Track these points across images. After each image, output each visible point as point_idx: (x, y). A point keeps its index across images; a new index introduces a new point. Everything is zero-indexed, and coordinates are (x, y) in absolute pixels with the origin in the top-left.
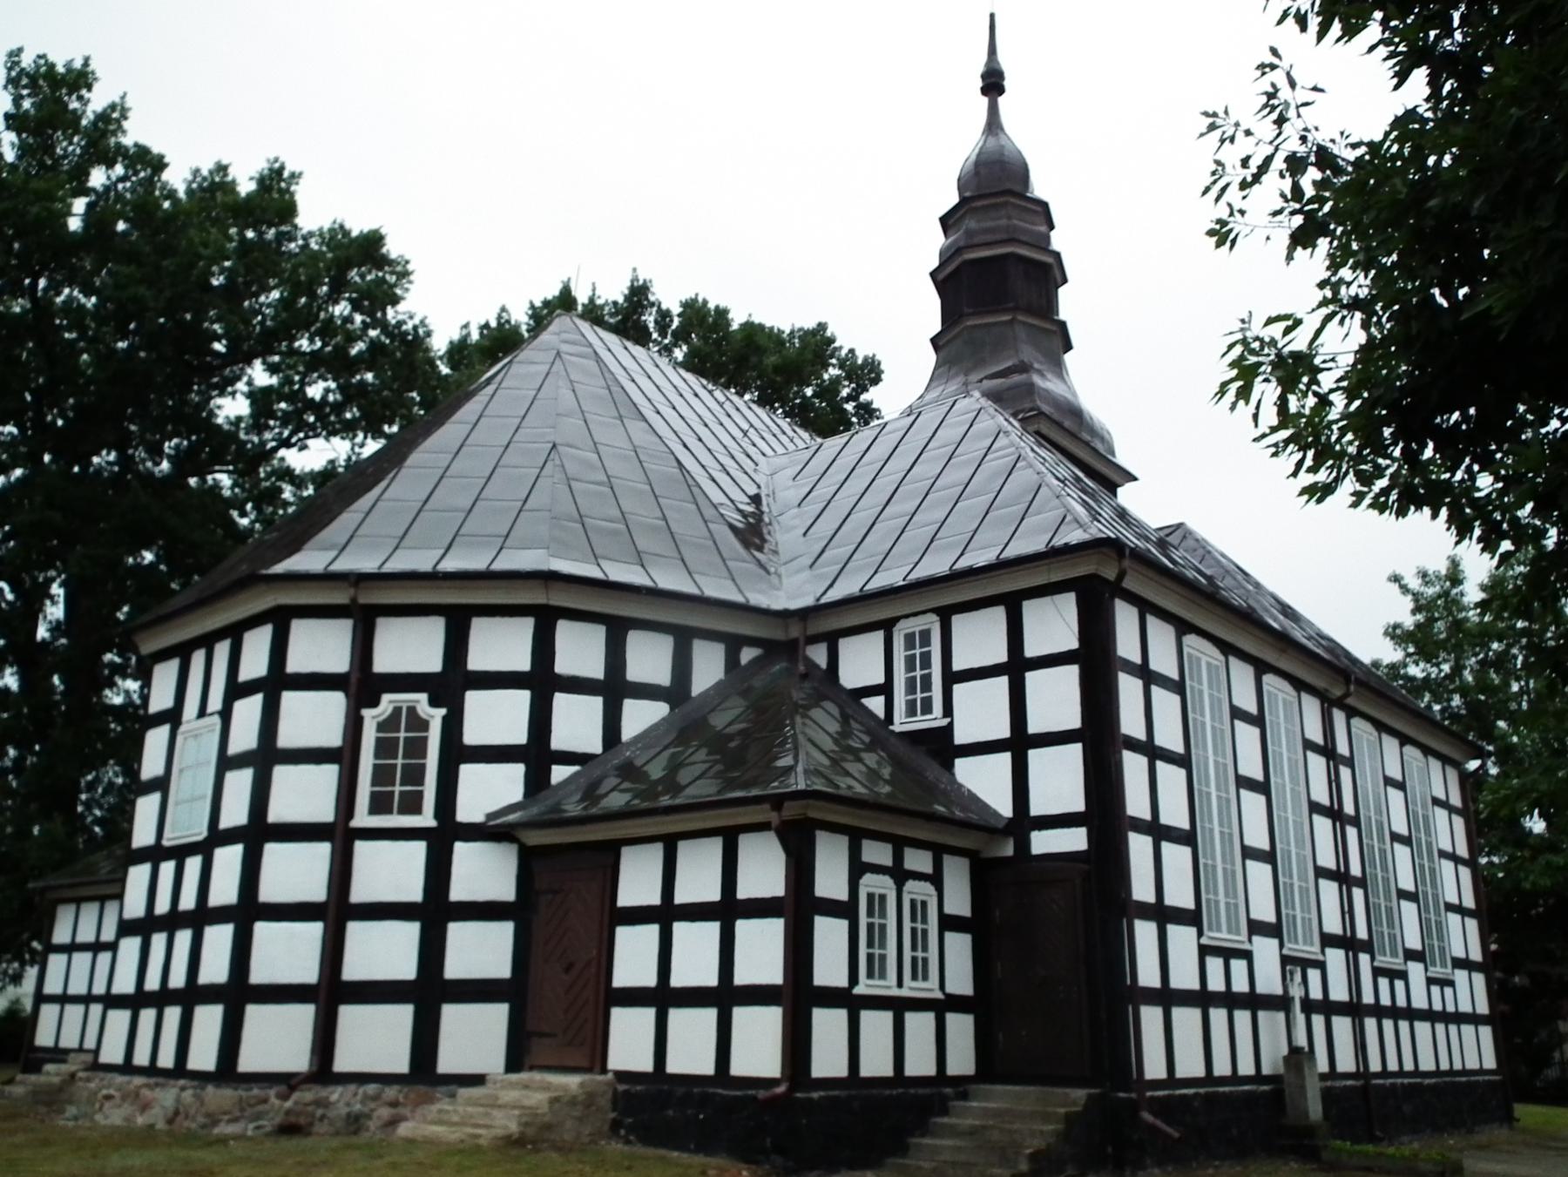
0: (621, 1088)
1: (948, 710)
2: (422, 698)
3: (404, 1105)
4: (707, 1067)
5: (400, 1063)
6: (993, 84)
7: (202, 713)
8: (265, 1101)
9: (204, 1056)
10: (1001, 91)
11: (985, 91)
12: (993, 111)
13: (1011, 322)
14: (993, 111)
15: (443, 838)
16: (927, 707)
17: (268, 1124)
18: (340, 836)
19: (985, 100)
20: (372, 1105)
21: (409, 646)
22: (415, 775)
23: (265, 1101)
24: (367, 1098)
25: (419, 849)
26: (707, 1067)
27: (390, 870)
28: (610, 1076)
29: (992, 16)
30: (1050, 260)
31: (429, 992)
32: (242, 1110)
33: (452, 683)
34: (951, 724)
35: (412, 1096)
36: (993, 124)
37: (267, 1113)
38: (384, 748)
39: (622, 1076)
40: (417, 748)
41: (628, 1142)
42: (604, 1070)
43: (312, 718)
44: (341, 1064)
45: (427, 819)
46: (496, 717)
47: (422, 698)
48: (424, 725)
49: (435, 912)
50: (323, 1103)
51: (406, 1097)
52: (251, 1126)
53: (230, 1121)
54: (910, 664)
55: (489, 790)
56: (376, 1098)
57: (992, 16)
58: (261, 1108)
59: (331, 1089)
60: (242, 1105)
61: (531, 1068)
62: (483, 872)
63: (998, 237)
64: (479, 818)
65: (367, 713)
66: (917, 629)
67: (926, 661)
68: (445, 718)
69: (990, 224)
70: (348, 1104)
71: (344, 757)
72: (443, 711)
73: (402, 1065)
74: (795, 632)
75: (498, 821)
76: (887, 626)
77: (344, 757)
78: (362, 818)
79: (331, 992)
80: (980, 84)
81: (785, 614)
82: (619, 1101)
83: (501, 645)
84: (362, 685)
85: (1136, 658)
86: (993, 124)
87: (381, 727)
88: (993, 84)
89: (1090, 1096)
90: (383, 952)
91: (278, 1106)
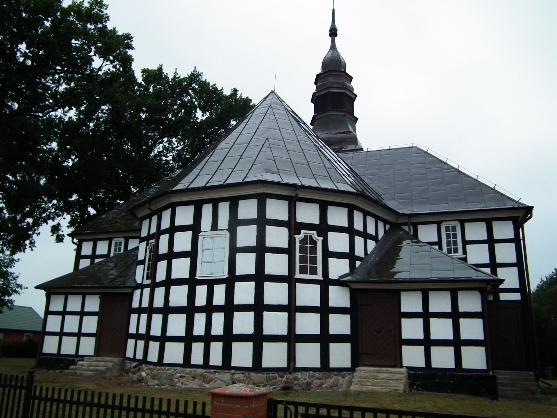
0: (411, 372)
1: (465, 252)
2: (315, 233)
3: (322, 379)
4: (55, 351)
5: (317, 364)
6: (333, 33)
7: (215, 227)
8: (276, 378)
9: (153, 356)
10: (336, 35)
11: (330, 35)
12: (333, 42)
13: (345, 115)
14: (333, 42)
15: (325, 284)
16: (456, 251)
17: (279, 387)
18: (290, 280)
19: (331, 38)
20: (312, 379)
21: (308, 214)
22: (314, 260)
23: (276, 378)
24: (310, 377)
25: (317, 287)
26: (55, 351)
27: (308, 295)
28: (404, 370)
29: (334, 10)
30: (353, 97)
31: (325, 339)
32: (268, 382)
33: (323, 228)
34: (466, 257)
35: (324, 375)
36: (333, 47)
37: (277, 382)
38: (303, 250)
39: (409, 368)
40: (314, 250)
41: (418, 390)
42: (401, 366)
43: (277, 237)
44: (166, 361)
45: (319, 277)
46: (338, 242)
47: (315, 233)
48: (315, 243)
49: (324, 310)
50: (296, 379)
51: (323, 376)
52: (271, 387)
53: (263, 386)
54: (448, 236)
55: (338, 268)
56: (313, 377)
57: (334, 10)
58: (274, 381)
59: (297, 373)
60: (269, 379)
61: (363, 366)
62: (339, 297)
63: (339, 86)
64: (336, 278)
65: (297, 236)
66: (450, 226)
67: (455, 236)
68: (322, 241)
69: (338, 81)
70: (305, 379)
71: (289, 251)
72: (322, 238)
73: (181, 361)
74: (401, 221)
75: (344, 279)
76: (439, 224)
77: (289, 251)
78: (319, 277)
79: (292, 338)
80: (329, 33)
81: (403, 215)
82: (409, 377)
83: (248, 209)
84: (293, 226)
85: (361, 229)
86: (333, 47)
87: (301, 242)
88: (333, 33)
89: (119, 360)
90: (308, 324)
91: (282, 380)
